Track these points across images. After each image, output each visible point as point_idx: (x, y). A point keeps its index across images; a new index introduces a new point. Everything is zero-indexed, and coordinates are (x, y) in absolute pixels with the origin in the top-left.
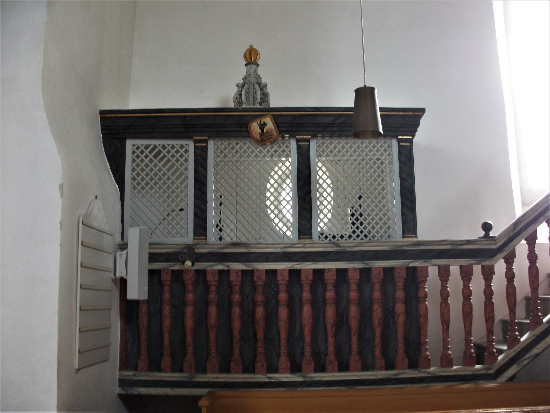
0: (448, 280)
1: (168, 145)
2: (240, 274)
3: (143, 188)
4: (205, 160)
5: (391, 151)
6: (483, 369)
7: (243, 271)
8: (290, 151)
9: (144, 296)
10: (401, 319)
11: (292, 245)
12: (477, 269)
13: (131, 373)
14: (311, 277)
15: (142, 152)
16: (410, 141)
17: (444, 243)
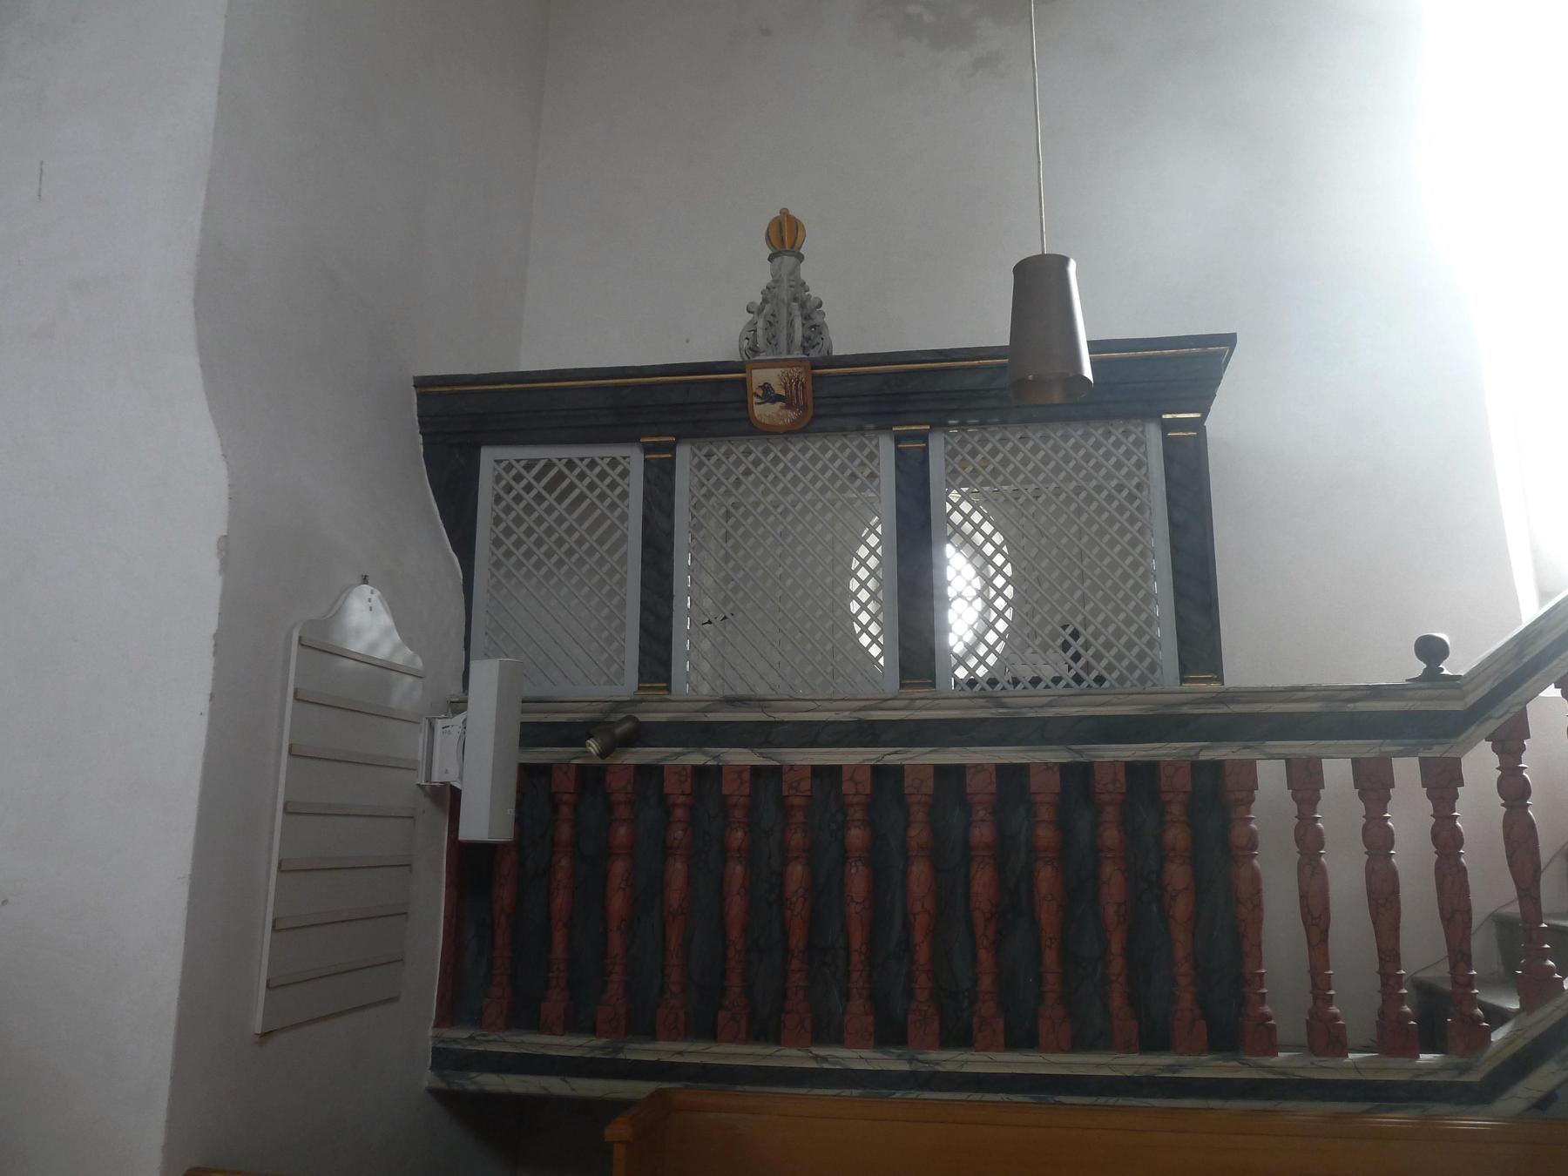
0: (1319, 798)
1: (582, 460)
2: (746, 776)
3: (519, 565)
4: (670, 493)
5: (1145, 454)
6: (1443, 1068)
7: (756, 771)
9: (503, 832)
10: (1181, 907)
11: (881, 703)
12: (1407, 771)
13: (463, 1034)
14: (928, 788)
15: (518, 478)
16: (1198, 425)
17: (1300, 695)
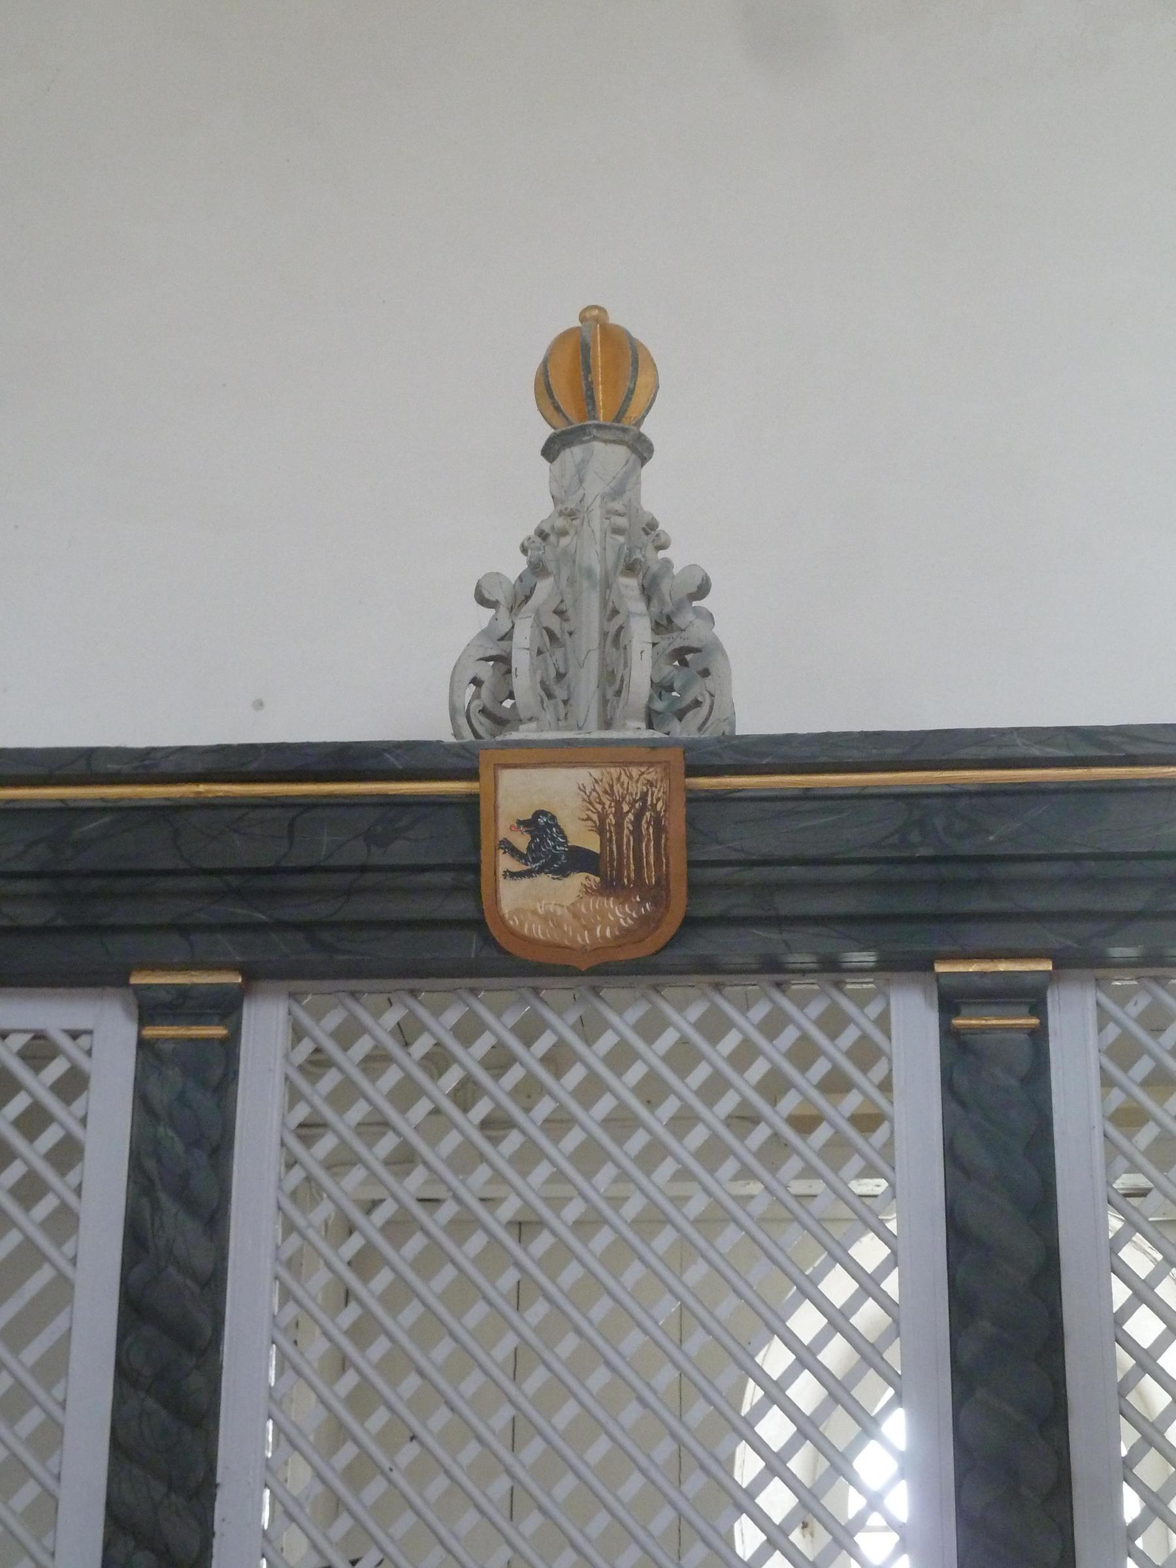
4: (219, 1150)
8: (886, 1086)
